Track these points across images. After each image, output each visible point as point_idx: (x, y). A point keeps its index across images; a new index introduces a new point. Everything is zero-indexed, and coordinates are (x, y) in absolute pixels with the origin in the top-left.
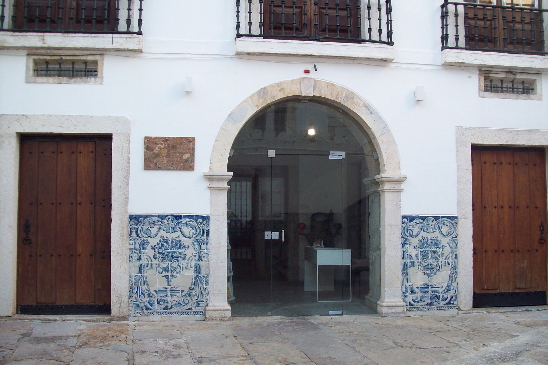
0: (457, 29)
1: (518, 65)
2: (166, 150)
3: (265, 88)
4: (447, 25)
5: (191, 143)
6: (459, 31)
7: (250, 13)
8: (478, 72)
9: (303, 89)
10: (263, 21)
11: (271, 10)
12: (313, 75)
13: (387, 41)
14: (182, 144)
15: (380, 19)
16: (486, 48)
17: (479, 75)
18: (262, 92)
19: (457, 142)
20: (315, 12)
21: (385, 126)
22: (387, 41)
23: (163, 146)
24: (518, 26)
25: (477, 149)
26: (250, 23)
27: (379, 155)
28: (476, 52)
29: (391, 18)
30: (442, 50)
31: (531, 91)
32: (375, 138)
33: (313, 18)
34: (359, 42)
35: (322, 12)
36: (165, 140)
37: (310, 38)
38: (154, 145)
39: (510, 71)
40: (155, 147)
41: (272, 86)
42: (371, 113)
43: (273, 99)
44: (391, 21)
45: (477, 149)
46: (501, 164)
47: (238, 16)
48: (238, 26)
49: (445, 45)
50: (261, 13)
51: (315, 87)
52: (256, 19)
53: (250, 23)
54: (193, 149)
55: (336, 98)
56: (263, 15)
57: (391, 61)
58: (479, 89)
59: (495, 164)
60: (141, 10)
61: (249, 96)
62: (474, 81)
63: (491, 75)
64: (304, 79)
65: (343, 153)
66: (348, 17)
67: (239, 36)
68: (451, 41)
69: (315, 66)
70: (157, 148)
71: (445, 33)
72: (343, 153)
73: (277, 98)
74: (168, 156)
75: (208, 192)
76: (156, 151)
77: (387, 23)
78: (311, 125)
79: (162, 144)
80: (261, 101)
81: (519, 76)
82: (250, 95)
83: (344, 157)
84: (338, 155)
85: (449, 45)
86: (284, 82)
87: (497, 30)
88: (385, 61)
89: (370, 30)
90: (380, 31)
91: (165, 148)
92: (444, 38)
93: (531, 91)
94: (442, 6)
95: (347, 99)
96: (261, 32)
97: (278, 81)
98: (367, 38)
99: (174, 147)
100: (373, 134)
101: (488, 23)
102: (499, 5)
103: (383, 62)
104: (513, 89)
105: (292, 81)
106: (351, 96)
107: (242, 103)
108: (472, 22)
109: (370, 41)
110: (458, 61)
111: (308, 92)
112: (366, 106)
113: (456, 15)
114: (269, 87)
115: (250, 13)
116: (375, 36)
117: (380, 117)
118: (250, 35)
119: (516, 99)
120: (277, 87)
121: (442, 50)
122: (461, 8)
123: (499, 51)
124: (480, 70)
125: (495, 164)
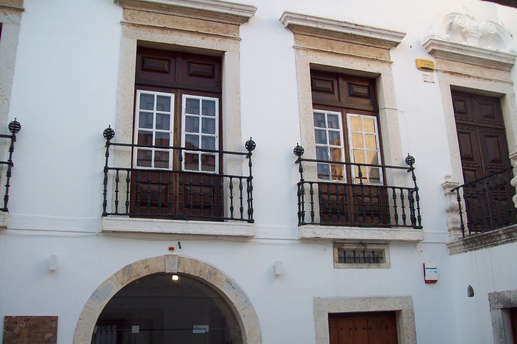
0: (313, 206)
1: (368, 237)
2: (27, 330)
3: (130, 265)
4: (303, 203)
5: (54, 322)
6: (314, 207)
7: (117, 191)
8: (332, 245)
9: (167, 266)
10: (129, 199)
11: (137, 186)
12: (177, 252)
13: (247, 219)
14: (44, 323)
15: (241, 198)
16: (340, 223)
17: (334, 247)
18: (127, 270)
19: (314, 312)
20: (180, 191)
21: (247, 301)
22: (247, 219)
23: (24, 326)
24: (367, 199)
25: (333, 317)
26: (117, 202)
27: (241, 328)
28: (330, 227)
29: (251, 197)
30: (299, 226)
31: (380, 259)
32: (237, 311)
33: (178, 195)
34: (222, 220)
35: (187, 189)
36: (27, 319)
37: (175, 217)
38: (15, 325)
39: (362, 242)
40: (16, 327)
41: (137, 263)
42: (233, 288)
43: (138, 275)
44: (252, 199)
45: (333, 317)
46: (356, 329)
47: (105, 194)
48: (105, 205)
49: (301, 221)
50: (128, 192)
51: (179, 263)
52: (123, 197)
53: (117, 202)
54: (56, 328)
55: (200, 274)
56: (129, 194)
57: (252, 237)
58: (334, 261)
59: (351, 329)
60: (8, 186)
61: (113, 273)
62: (328, 255)
63: (344, 247)
64: (168, 255)
65: (207, 327)
66: (211, 196)
67: (105, 214)
68: (307, 218)
69: (179, 243)
70: (18, 328)
71: (301, 210)
72: (207, 327)
73: (141, 276)
74: (29, 336)
75: (120, 27)
76: (16, 331)
77: (248, 201)
78: (176, 283)
79: (23, 324)
80: (126, 278)
81: (369, 247)
82: (115, 272)
83: (207, 331)
84: (202, 329)
85: (305, 221)
86: (149, 259)
87: (349, 205)
88: (246, 237)
89: (232, 209)
90: (242, 210)
91: (26, 327)
92: (301, 214)
93: (380, 259)
94: (299, 184)
95: (210, 275)
96: (127, 211)
97: (144, 258)
98: (229, 216)
99: (35, 326)
100: (235, 308)
101: (340, 197)
102: (350, 183)
103: (244, 239)
104: (364, 258)
105: (157, 258)
106: (214, 272)
107: (106, 281)
108: (326, 197)
109: (232, 219)
110: (314, 236)
111: (172, 269)
112: (229, 282)
113: (312, 193)
114: (134, 264)
115: (117, 191)
116: (237, 214)
117: (242, 292)
118: (116, 214)
119: (367, 268)
120: (141, 264)
121: (299, 226)
122: (315, 187)
123: (351, 226)
124: (334, 243)
125: (351, 329)
